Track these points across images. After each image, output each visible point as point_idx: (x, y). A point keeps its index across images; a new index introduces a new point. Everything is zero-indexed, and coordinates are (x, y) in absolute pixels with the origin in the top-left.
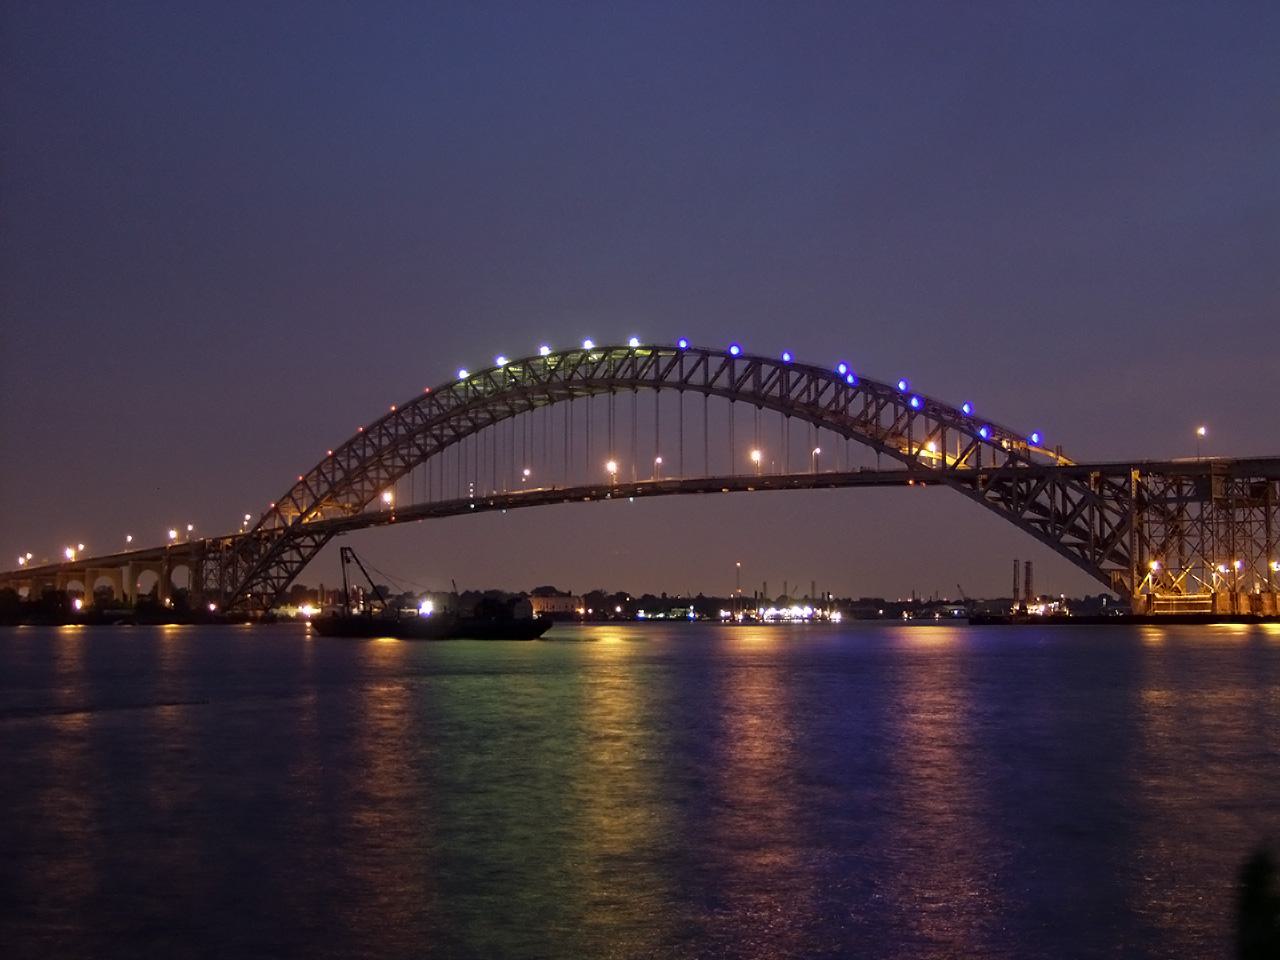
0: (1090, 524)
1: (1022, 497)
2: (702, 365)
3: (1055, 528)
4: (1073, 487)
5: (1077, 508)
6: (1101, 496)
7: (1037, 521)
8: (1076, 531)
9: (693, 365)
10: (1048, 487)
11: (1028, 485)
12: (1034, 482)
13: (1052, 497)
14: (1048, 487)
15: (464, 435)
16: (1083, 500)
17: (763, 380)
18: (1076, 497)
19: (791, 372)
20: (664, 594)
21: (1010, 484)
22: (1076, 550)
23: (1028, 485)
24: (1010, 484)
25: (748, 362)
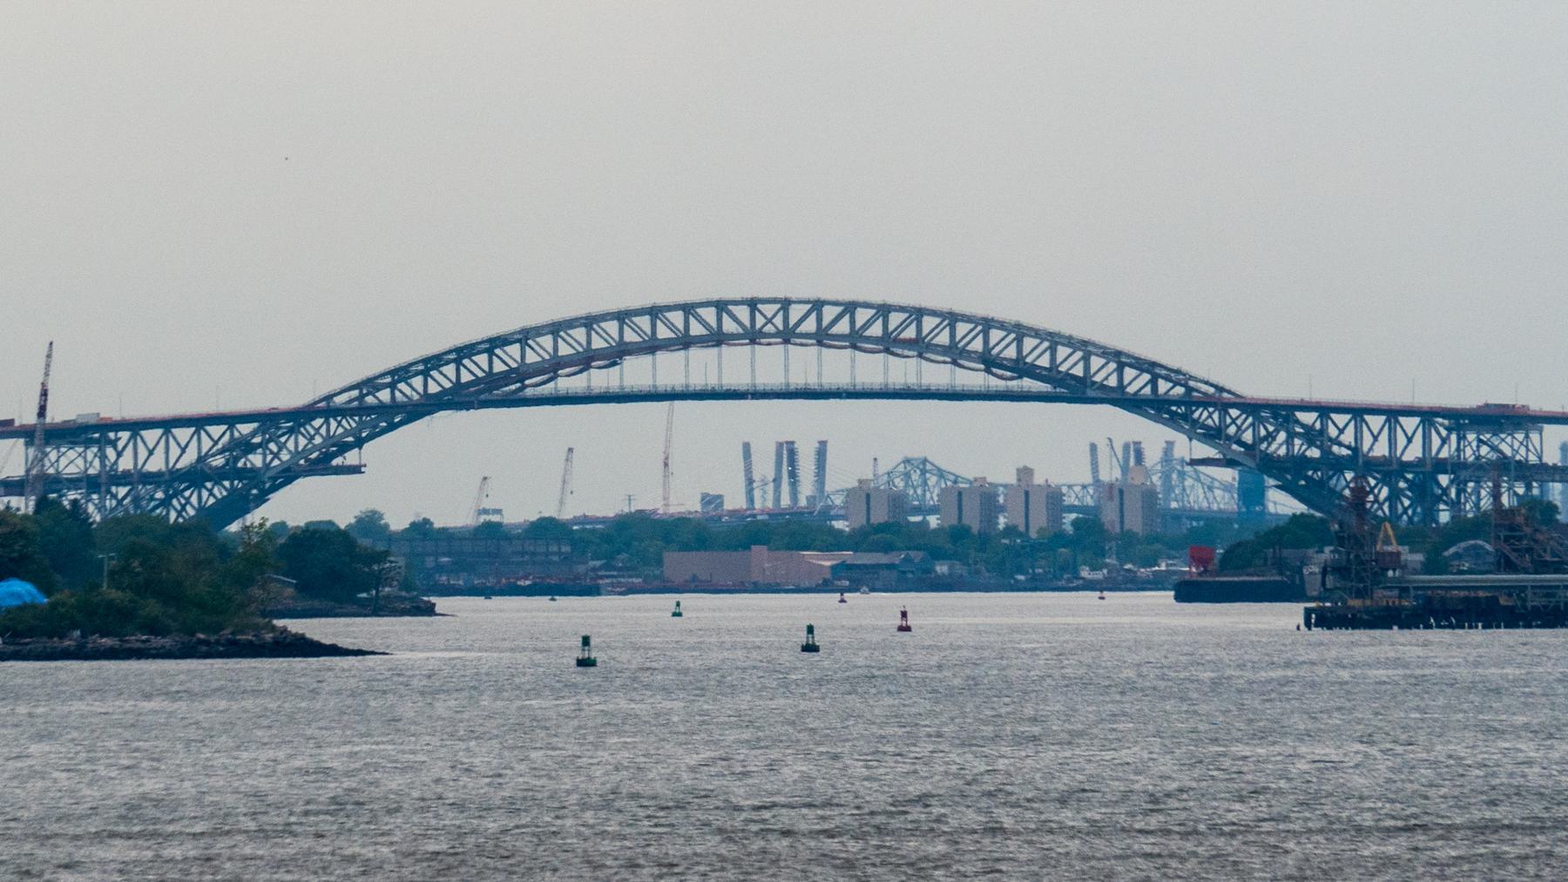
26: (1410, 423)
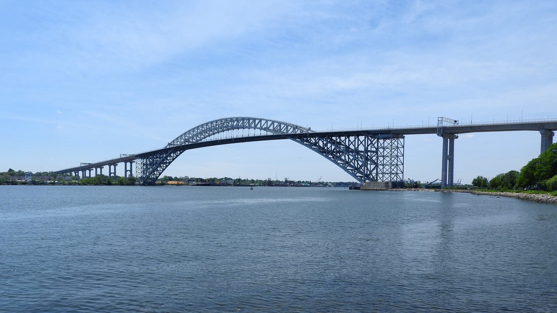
0: (354, 164)
1: (338, 157)
2: (260, 123)
3: (355, 172)
4: (351, 155)
5: (351, 161)
6: (358, 158)
7: (341, 163)
8: (341, 160)
9: (264, 123)
10: (344, 155)
11: (340, 154)
12: (341, 153)
13: (345, 157)
14: (344, 155)
15: (207, 137)
16: (362, 164)
17: (254, 123)
18: (351, 157)
19: (98, 168)
20: (257, 180)
21: (335, 154)
22: (341, 165)
23: (340, 154)
24: (335, 154)
25: (278, 124)
26: (362, 138)
